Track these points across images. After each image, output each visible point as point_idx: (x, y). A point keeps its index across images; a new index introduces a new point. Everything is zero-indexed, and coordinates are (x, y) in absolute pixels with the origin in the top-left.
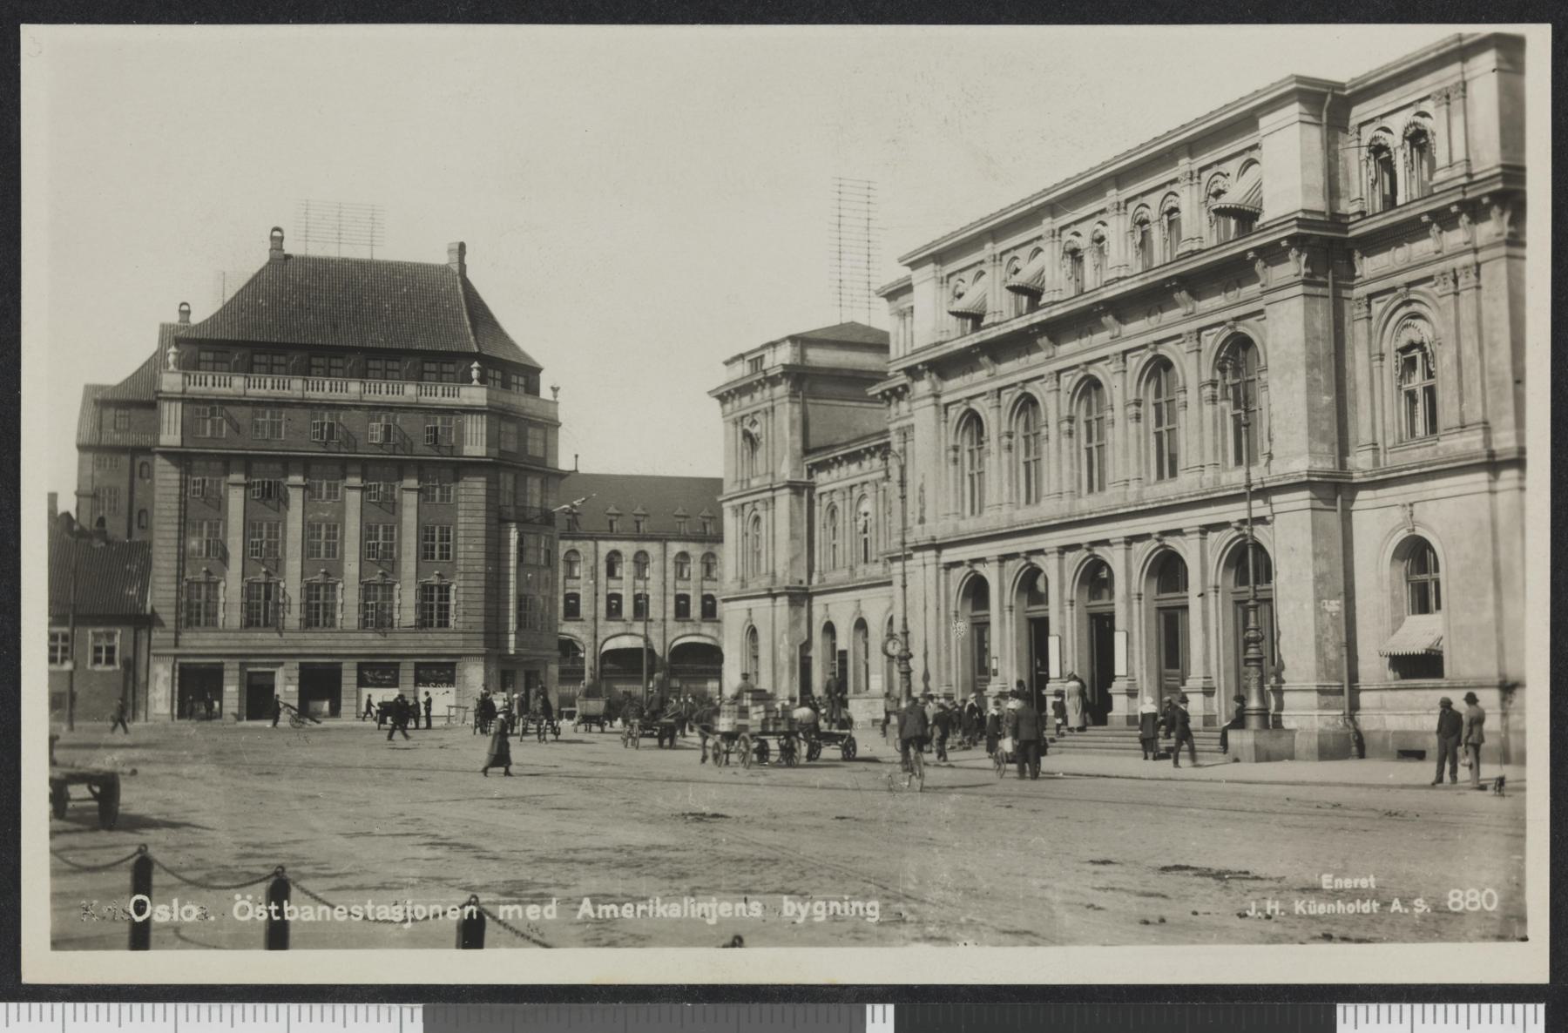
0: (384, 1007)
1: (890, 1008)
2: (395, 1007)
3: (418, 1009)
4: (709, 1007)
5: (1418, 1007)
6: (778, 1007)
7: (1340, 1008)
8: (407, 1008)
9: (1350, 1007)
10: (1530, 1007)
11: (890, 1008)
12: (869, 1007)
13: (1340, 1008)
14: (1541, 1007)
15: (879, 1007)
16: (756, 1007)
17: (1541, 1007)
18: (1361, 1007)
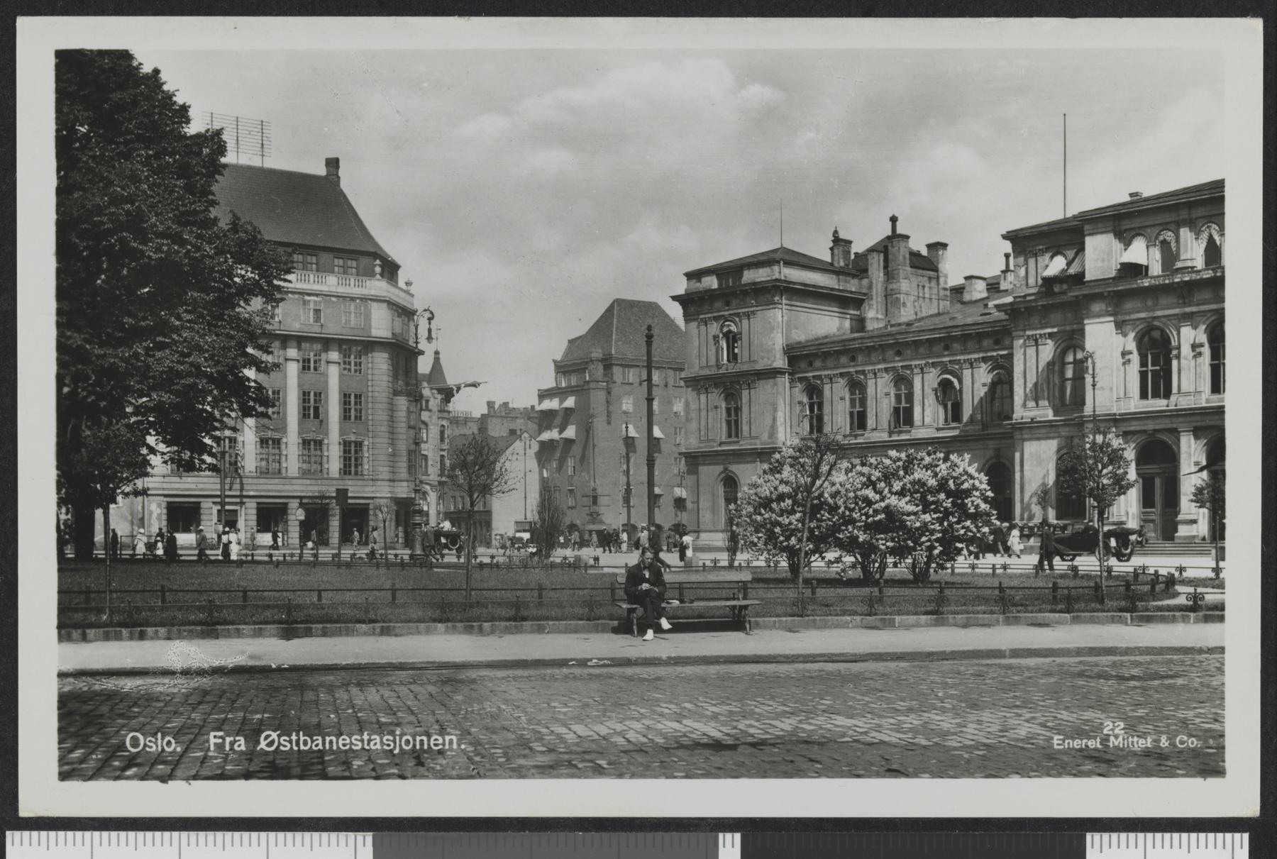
0: (342, 835)
1: (738, 836)
2: (351, 835)
3: (369, 837)
4: (596, 836)
5: (1150, 835)
6: (650, 835)
7: (1089, 836)
8: (360, 836)
9: (1097, 836)
10: (1237, 836)
11: (738, 836)
12: (721, 835)
13: (1089, 836)
14: (1246, 836)
15: (729, 836)
16: (632, 835)
17: (1246, 836)
18: (1106, 836)
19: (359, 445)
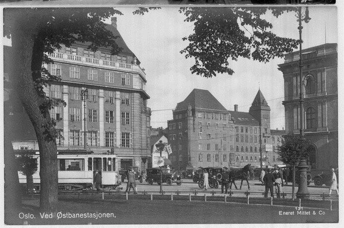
19: (128, 134)
